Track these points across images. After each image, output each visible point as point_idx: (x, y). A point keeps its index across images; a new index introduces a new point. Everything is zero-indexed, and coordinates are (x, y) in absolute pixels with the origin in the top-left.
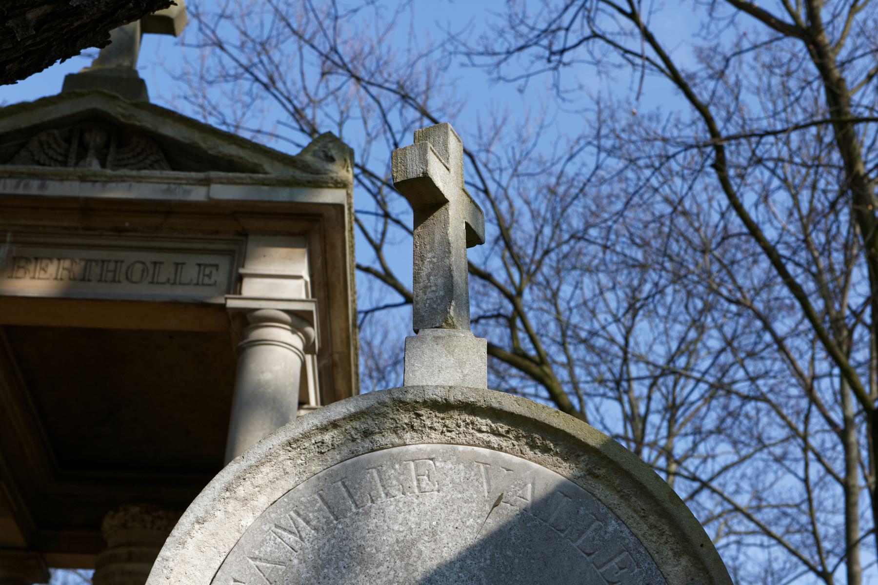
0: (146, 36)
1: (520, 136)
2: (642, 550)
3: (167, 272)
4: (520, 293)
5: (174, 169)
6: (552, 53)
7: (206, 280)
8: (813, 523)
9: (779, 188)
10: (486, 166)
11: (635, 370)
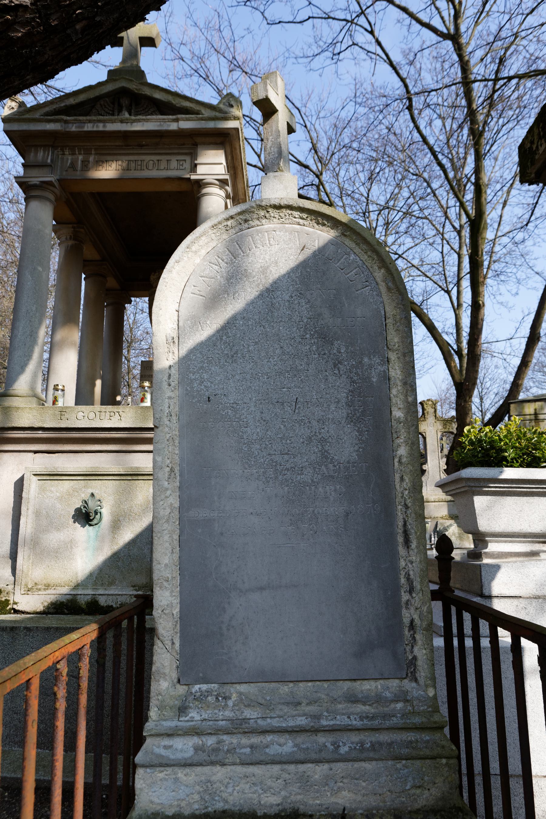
0: (144, 49)
1: (320, 99)
2: (365, 267)
3: (163, 165)
4: (321, 174)
5: (162, 115)
6: (334, 55)
7: (181, 167)
8: (444, 271)
9: (436, 118)
10: (305, 114)
11: (372, 208)
